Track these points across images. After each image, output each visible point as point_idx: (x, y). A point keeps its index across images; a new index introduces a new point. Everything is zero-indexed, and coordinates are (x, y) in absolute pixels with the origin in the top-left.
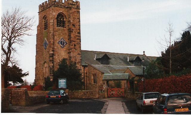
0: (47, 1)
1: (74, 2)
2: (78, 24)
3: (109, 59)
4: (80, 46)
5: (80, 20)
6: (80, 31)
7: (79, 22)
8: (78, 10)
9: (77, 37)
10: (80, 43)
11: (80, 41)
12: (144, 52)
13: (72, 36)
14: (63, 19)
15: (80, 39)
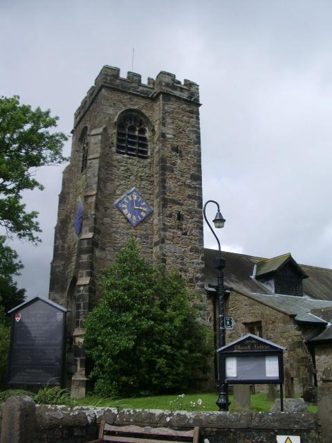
1: (179, 83)
2: (192, 148)
5: (199, 138)
6: (199, 170)
9: (189, 192)
13: (170, 184)
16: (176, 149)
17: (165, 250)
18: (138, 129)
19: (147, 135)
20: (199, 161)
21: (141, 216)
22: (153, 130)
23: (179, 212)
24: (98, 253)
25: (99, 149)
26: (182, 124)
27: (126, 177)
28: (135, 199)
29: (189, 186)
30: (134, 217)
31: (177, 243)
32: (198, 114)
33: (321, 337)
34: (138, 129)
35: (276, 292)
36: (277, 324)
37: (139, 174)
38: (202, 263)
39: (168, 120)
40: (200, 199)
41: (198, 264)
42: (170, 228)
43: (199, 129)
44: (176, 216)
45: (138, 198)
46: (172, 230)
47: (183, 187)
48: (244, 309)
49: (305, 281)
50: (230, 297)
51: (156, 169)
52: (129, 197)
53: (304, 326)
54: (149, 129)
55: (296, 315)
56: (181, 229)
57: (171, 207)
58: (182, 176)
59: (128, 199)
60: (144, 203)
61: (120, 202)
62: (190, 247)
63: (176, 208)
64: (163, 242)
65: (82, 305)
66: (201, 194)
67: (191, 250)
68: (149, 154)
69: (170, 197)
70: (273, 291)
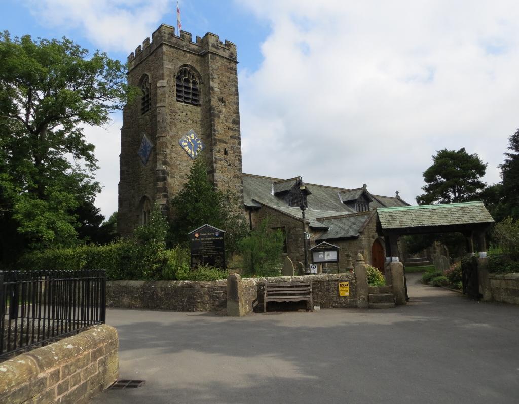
1: (221, 43)
2: (232, 99)
4: (241, 157)
5: (237, 90)
6: (238, 117)
8: (233, 65)
11: (239, 144)
12: (397, 193)
14: (194, 83)
15: (239, 138)
20: (238, 109)
27: (185, 121)
36: (297, 230)
43: (237, 83)
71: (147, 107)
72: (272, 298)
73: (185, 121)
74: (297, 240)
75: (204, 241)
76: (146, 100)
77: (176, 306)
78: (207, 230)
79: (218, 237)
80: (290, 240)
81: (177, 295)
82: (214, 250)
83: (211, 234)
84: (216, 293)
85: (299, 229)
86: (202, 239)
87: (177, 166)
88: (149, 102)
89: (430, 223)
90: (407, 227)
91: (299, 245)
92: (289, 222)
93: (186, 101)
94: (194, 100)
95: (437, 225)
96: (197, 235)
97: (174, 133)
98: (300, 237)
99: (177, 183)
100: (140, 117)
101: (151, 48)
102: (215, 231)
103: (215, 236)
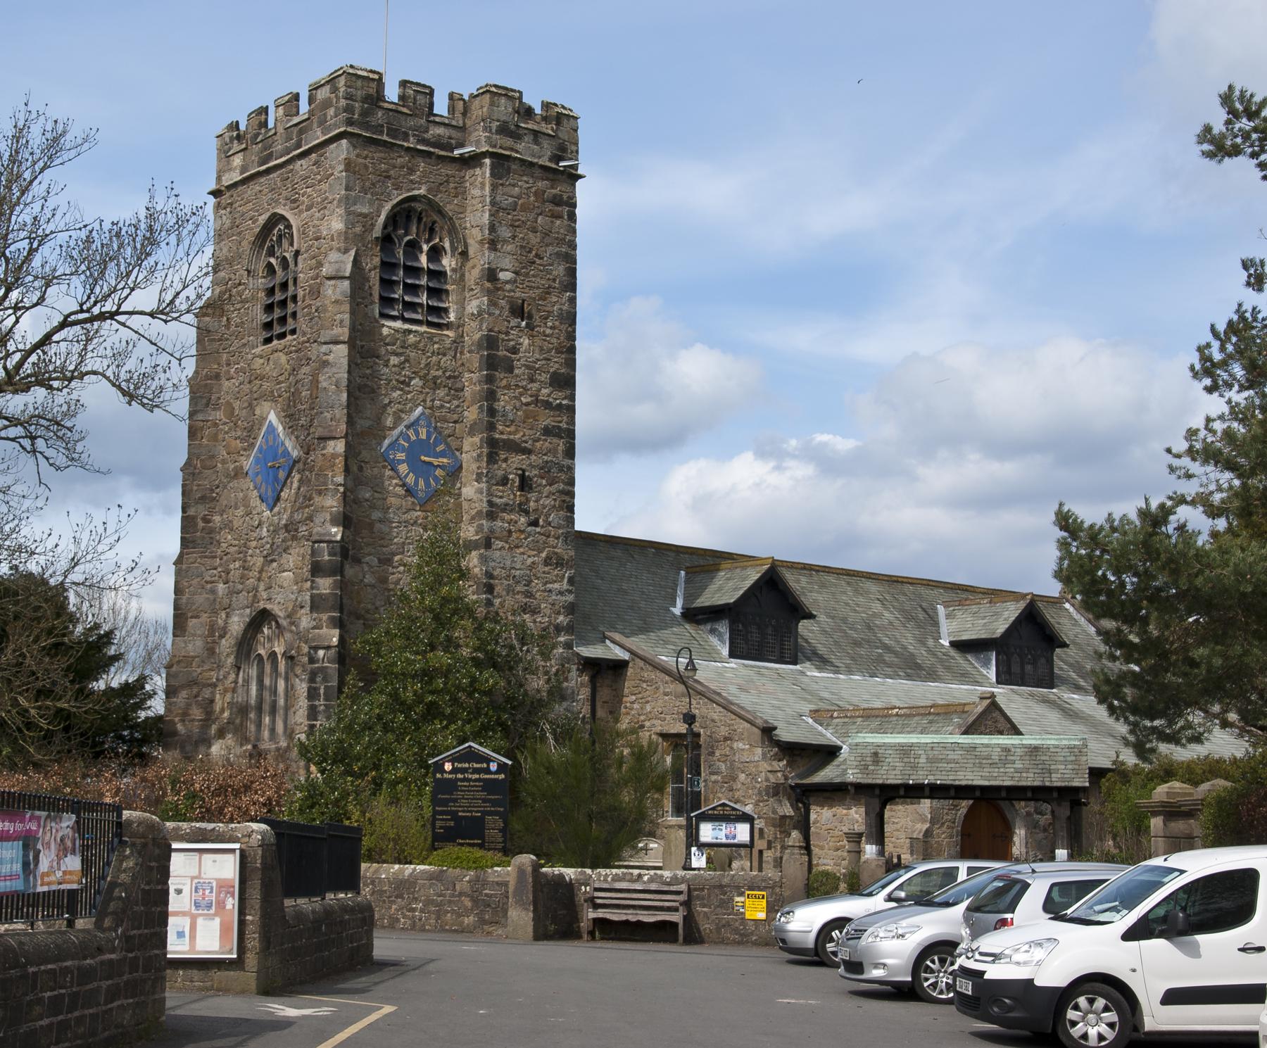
0: (296, 97)
1: (529, 112)
2: (556, 303)
3: (798, 611)
5: (572, 272)
6: (571, 364)
7: (571, 286)
9: (546, 420)
10: (571, 469)
13: (504, 402)
14: (435, 253)
16: (518, 311)
17: (492, 564)
18: (425, 247)
19: (448, 263)
20: (572, 337)
21: (436, 479)
22: (464, 254)
23: (524, 471)
24: (350, 571)
25: (347, 316)
26: (534, 239)
27: (403, 383)
28: (423, 436)
29: (547, 405)
30: (421, 482)
31: (517, 547)
32: (574, 206)
33: (827, 774)
34: (425, 247)
35: (733, 654)
36: (735, 745)
37: (433, 373)
38: (570, 592)
39: (505, 232)
40: (571, 434)
41: (561, 593)
42: (504, 510)
43: (575, 248)
44: (517, 480)
45: (429, 435)
46: (507, 517)
47: (532, 407)
48: (660, 702)
49: (804, 627)
50: (630, 671)
51: (474, 359)
52: (411, 433)
53: (795, 752)
54: (454, 249)
55: (775, 728)
56: (527, 512)
57: (506, 460)
58: (532, 380)
59: (408, 439)
60: (440, 448)
61: (391, 445)
62: (544, 555)
63: (516, 460)
64: (488, 544)
65: (322, 691)
66: (572, 421)
67: (547, 562)
68: (452, 317)
69: (504, 437)
70: (725, 651)
71: (283, 320)
72: (601, 913)
73: (403, 383)
74: (734, 779)
75: (464, 780)
76: (279, 296)
77: (398, 920)
78: (471, 756)
79: (496, 773)
80: (714, 778)
81: (400, 896)
82: (484, 801)
83: (478, 766)
84: (486, 895)
85: (741, 745)
86: (460, 776)
87: (371, 525)
88: (291, 307)
89: (951, 777)
90: (899, 782)
91: (737, 794)
92: (713, 721)
93: (407, 315)
94: (433, 310)
95: (964, 783)
96: (448, 766)
97: (368, 423)
98: (743, 772)
99: (369, 579)
100: (257, 351)
101: (301, 132)
102: (488, 760)
103: (488, 771)
